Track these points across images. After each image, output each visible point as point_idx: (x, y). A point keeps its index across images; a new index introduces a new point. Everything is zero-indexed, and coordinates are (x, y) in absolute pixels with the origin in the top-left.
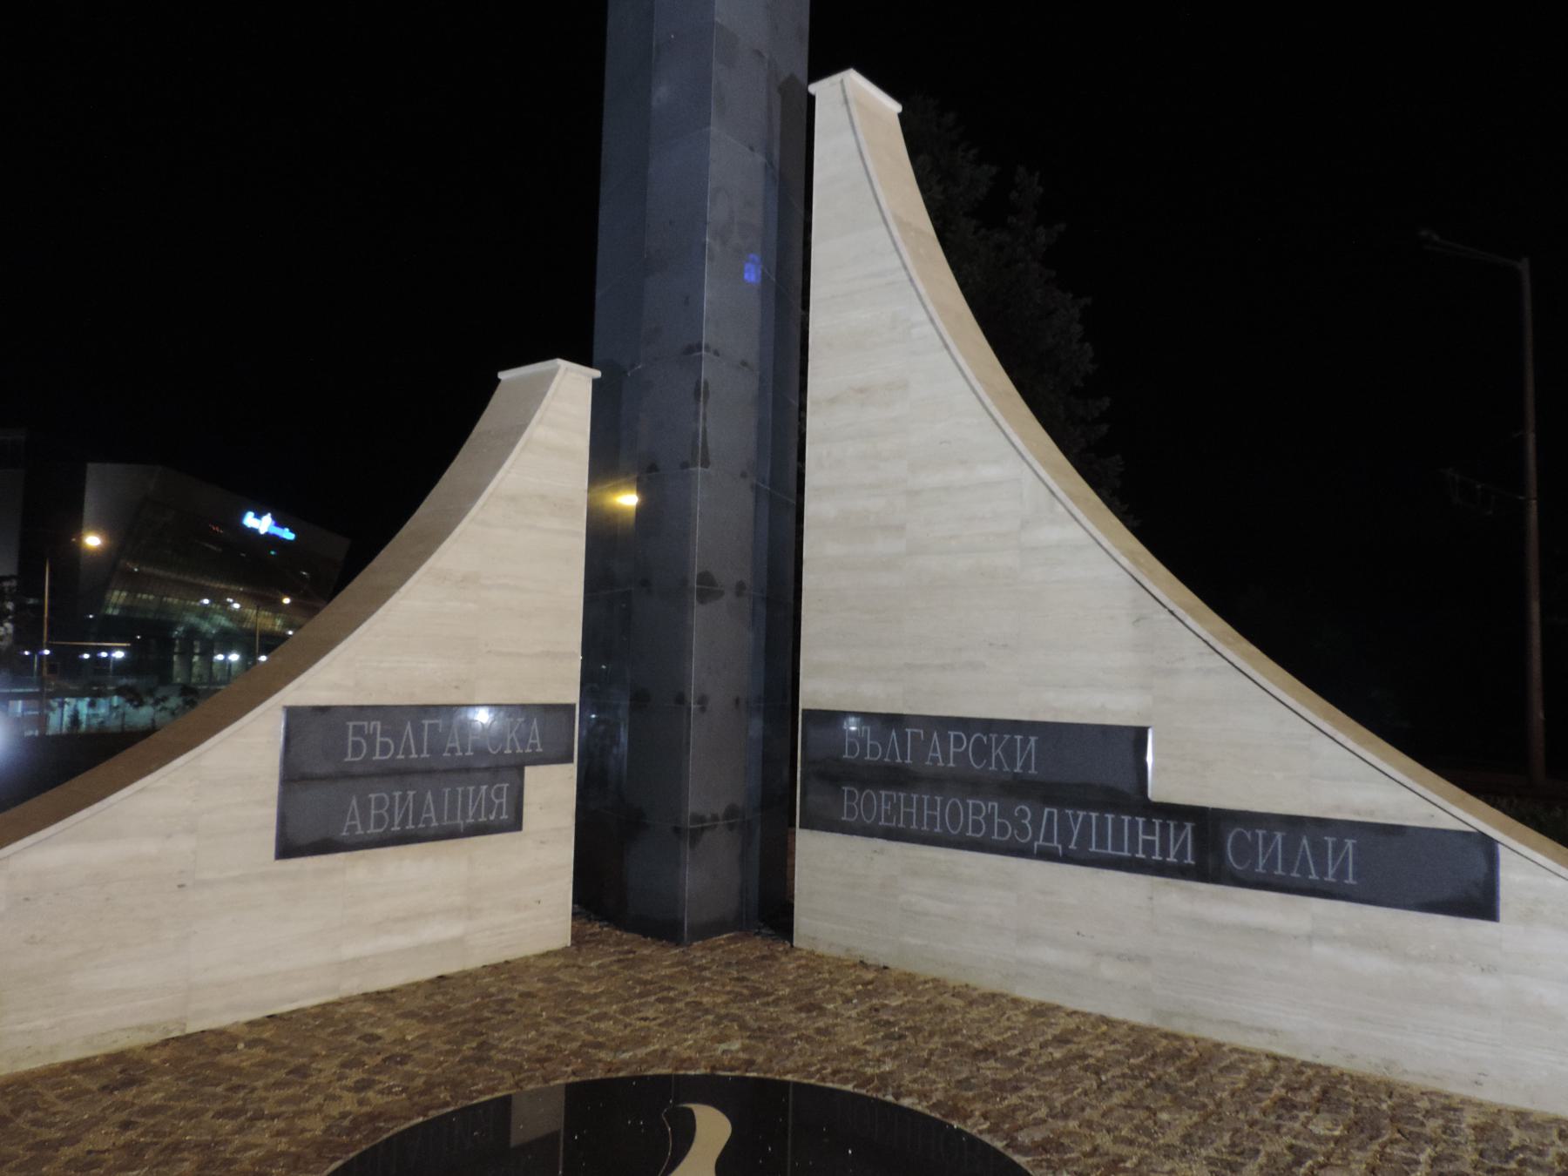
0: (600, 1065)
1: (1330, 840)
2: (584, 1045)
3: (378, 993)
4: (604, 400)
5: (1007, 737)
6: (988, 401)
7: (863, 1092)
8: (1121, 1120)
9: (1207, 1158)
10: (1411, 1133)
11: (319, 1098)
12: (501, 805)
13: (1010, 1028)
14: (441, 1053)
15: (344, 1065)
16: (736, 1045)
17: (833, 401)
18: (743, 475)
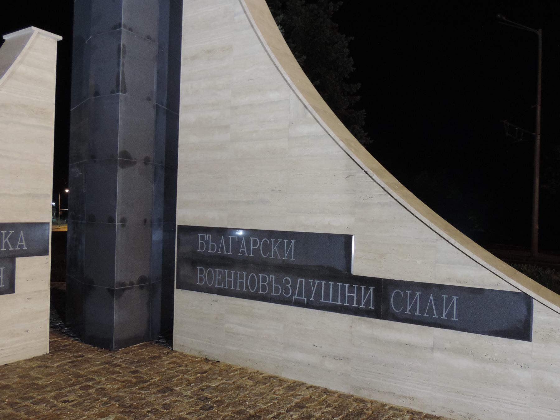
5: (280, 240)
6: (273, 56)
13: (274, 399)
17: (194, 58)
18: (149, 99)
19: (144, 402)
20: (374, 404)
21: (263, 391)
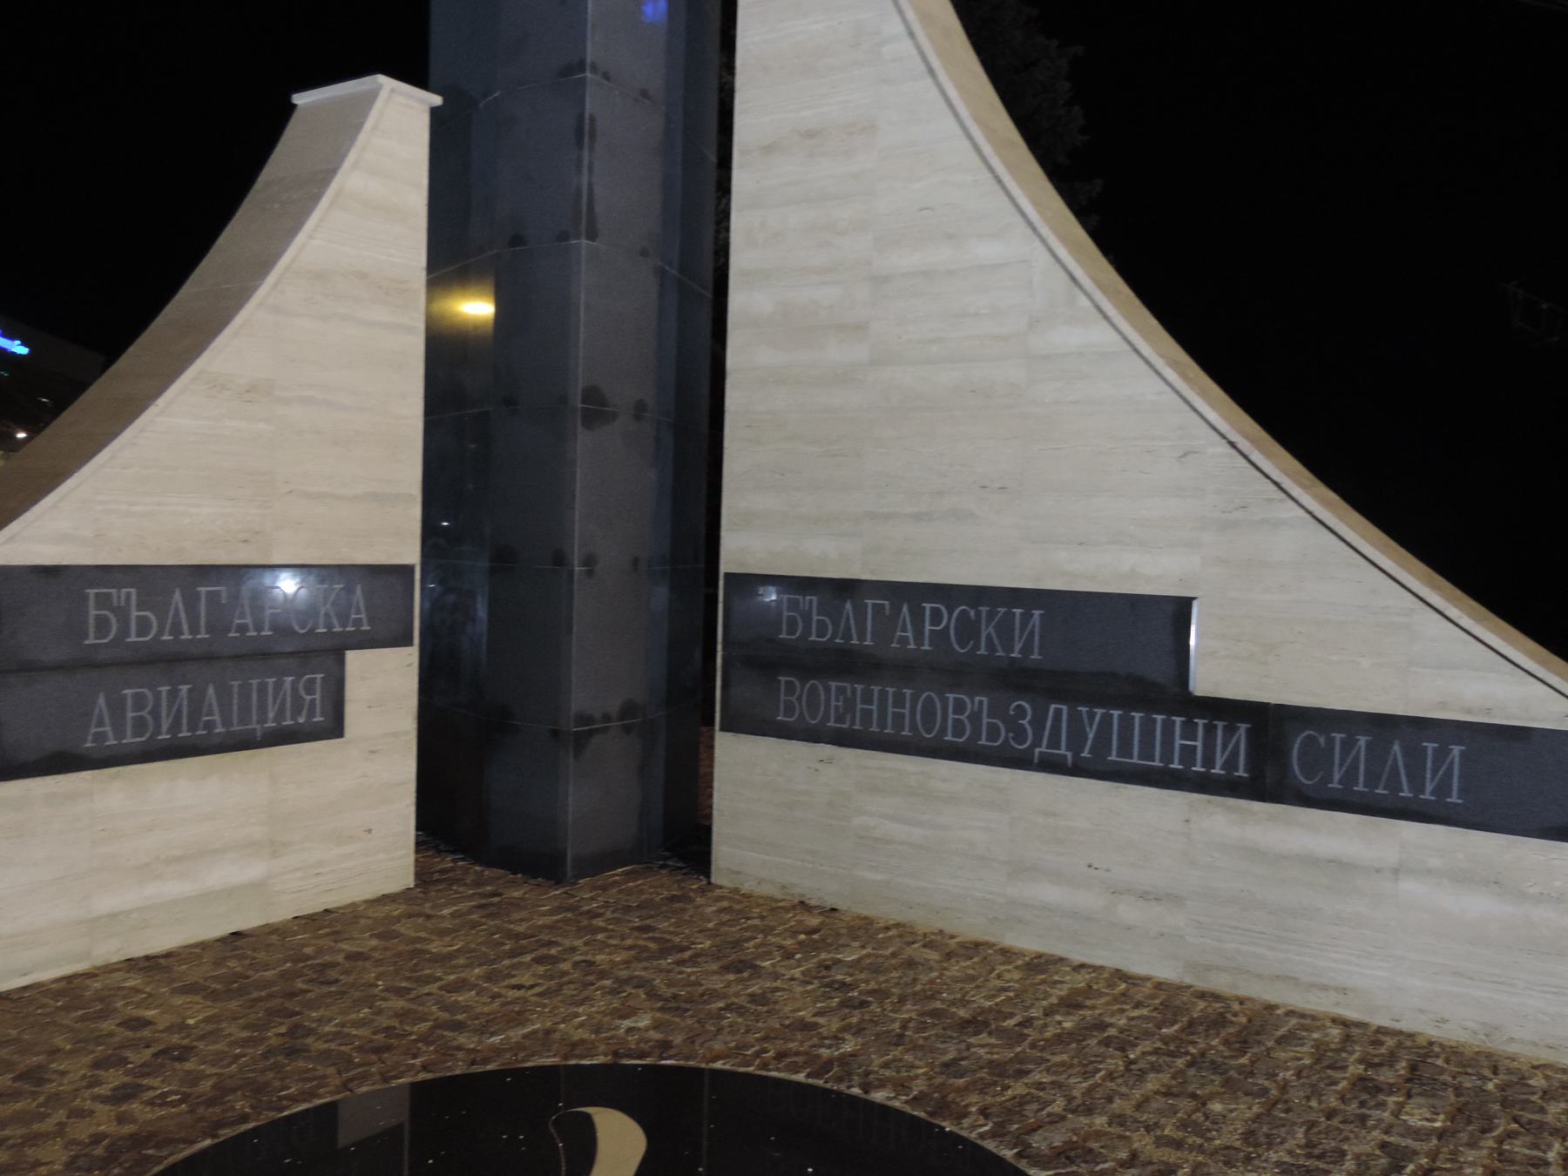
0: (460, 1055)
1: (1430, 746)
2: (439, 1025)
3: (147, 958)
4: (447, 136)
5: (1002, 610)
6: (988, 150)
7: (820, 1082)
8: (1160, 1112)
9: (1278, 1164)
10: (1530, 1122)
11: (60, 1115)
12: (313, 701)
14: (235, 1043)
15: (97, 1065)
16: (644, 1021)
18: (644, 253)
19: (701, 989)
20: (1248, 1005)
21: (971, 972)
